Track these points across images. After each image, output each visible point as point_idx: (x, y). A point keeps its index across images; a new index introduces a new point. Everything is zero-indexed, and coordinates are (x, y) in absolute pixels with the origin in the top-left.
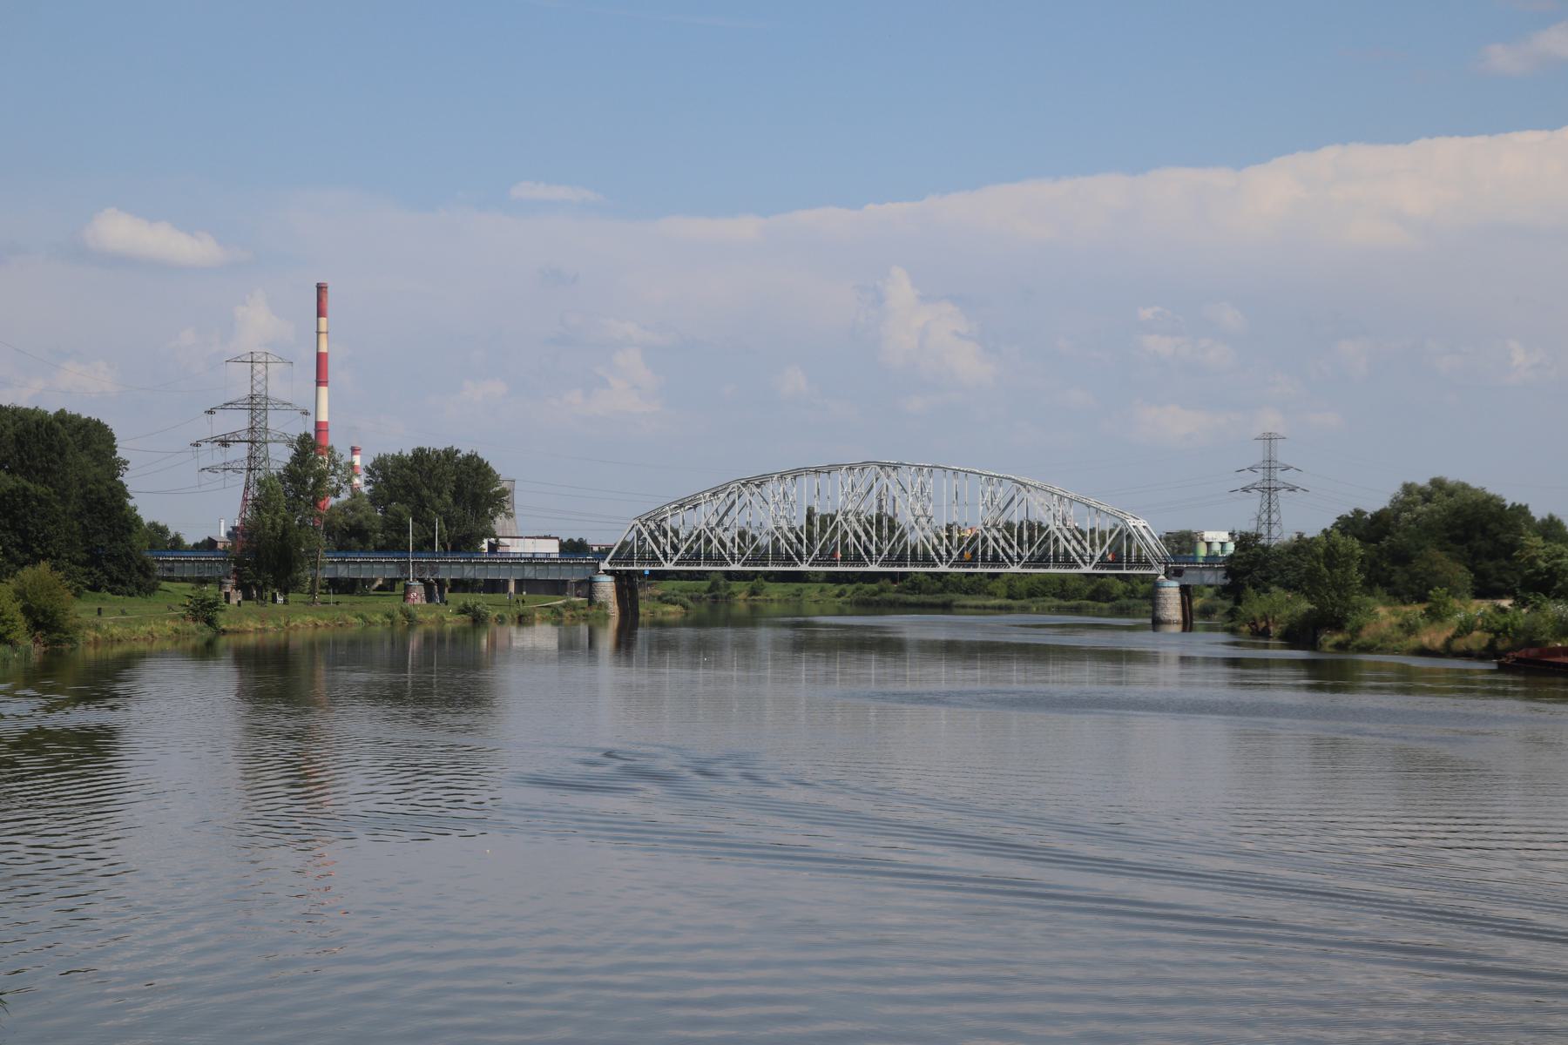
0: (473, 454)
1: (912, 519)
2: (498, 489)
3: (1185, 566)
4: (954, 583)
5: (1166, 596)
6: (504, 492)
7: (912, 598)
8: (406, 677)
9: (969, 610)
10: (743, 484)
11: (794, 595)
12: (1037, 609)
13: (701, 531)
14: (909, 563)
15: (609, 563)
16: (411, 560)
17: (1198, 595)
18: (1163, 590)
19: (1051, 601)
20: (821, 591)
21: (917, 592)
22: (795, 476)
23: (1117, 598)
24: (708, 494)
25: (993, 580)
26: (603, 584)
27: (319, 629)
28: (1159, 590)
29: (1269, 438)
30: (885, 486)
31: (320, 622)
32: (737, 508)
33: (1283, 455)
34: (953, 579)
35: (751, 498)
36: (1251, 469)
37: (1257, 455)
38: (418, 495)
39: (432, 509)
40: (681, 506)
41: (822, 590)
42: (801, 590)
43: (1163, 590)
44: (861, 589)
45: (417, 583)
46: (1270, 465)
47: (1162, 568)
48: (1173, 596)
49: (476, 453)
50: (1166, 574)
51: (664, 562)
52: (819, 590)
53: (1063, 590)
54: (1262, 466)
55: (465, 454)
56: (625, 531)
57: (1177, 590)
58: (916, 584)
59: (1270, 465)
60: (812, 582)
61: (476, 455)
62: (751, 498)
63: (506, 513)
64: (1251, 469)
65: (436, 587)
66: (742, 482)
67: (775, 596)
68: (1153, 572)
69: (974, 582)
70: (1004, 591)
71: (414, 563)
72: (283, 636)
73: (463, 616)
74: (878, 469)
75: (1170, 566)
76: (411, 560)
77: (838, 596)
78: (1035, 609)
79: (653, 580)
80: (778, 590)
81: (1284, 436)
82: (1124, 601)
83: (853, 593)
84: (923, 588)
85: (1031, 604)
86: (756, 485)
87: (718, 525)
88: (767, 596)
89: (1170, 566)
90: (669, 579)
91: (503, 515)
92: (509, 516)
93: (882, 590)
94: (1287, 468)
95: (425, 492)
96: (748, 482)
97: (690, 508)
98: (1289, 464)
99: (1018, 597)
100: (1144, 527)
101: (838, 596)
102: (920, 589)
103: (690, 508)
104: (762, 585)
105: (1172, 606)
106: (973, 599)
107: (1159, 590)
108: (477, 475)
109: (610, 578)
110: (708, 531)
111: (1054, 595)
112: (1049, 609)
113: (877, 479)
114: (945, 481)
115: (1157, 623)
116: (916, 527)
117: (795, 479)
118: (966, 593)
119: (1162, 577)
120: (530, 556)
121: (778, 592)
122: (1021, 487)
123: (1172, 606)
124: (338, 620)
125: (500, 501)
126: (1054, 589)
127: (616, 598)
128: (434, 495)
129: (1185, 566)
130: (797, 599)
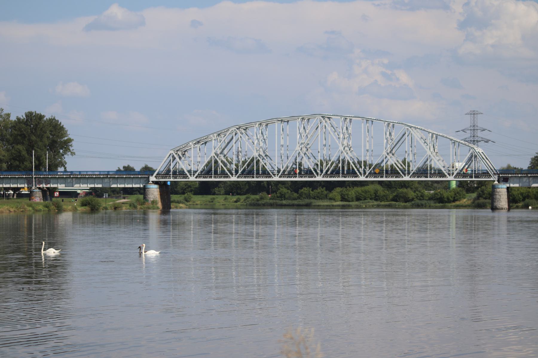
0: (53, 118)
1: (342, 148)
2: (66, 138)
3: (510, 175)
4: (305, 194)
5: (500, 194)
6: (70, 140)
7: (279, 202)
8: (475, 235)
9: (316, 207)
10: (237, 128)
11: (210, 202)
12: (366, 206)
13: (212, 157)
14: (341, 175)
15: (155, 177)
16: (34, 176)
17: (463, 197)
18: (498, 190)
19: (373, 202)
20: (225, 199)
21: (283, 199)
22: (267, 124)
23: (413, 200)
24: (215, 135)
25: (330, 192)
26: (152, 190)
27: (11, 214)
28: (496, 190)
29: (474, 114)
30: (324, 126)
31: (12, 210)
32: (234, 140)
33: (481, 122)
34: (305, 192)
35: (241, 136)
36: (463, 131)
37: (467, 122)
38: (29, 140)
39: (38, 148)
40: (198, 142)
41: (226, 199)
42: (214, 199)
43: (498, 190)
44: (249, 198)
45: (37, 190)
46: (474, 128)
47: (496, 177)
48: (504, 194)
49: (54, 117)
50: (499, 181)
51: (189, 176)
52: (224, 199)
53: (376, 196)
54: (470, 129)
55: (48, 118)
56: (165, 157)
57: (506, 190)
58: (282, 194)
59: (474, 128)
60: (217, 195)
61: (54, 119)
62: (241, 136)
63: (72, 153)
64: (463, 131)
65: (48, 192)
66: (237, 127)
67: (199, 202)
68: (492, 179)
69: (319, 193)
70: (339, 197)
71: (35, 178)
72: (80, 202)
73: (84, 207)
74: (321, 118)
75: (501, 175)
76: (34, 176)
77: (236, 202)
78: (364, 206)
79: (126, 194)
80: (200, 199)
81: (482, 112)
82: (418, 201)
83: (245, 200)
84: (286, 197)
85: (362, 204)
86: (244, 129)
87: (221, 153)
88: (194, 202)
89: (501, 175)
90: (135, 194)
91: (69, 153)
92: (73, 154)
93: (262, 198)
94: (484, 130)
95: (34, 138)
96: (240, 127)
97: (203, 144)
98: (485, 128)
99: (351, 200)
100: (482, 153)
101: (236, 202)
102: (285, 197)
103: (203, 144)
104: (190, 197)
105: (503, 201)
106: (323, 202)
107: (496, 190)
108: (55, 130)
109: (156, 186)
110: (216, 157)
111: (371, 199)
112: (373, 206)
113: (321, 123)
114: (363, 124)
115: (494, 208)
116: (344, 151)
117: (267, 126)
118: (314, 198)
119: (496, 182)
120: (106, 173)
121: (200, 200)
122: (409, 128)
123: (503, 201)
124: (20, 208)
125: (67, 146)
126: (371, 196)
127: (160, 198)
128: (38, 140)
129: (510, 175)
130: (212, 203)
